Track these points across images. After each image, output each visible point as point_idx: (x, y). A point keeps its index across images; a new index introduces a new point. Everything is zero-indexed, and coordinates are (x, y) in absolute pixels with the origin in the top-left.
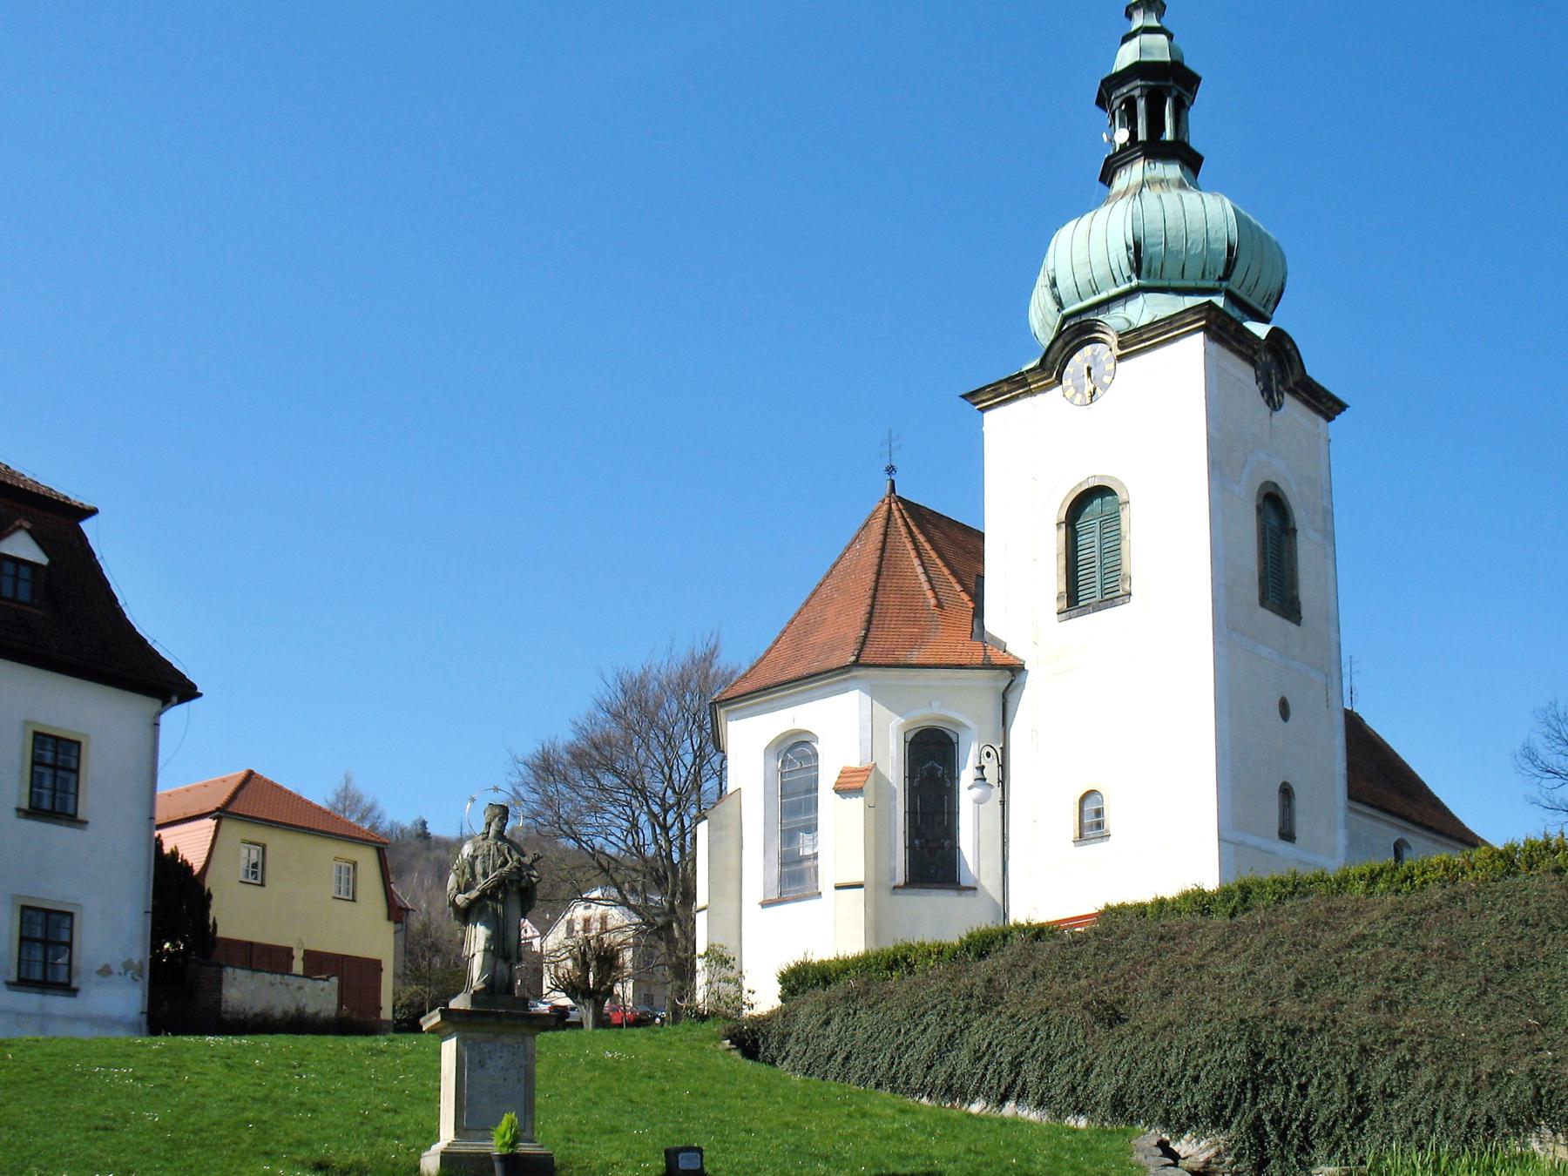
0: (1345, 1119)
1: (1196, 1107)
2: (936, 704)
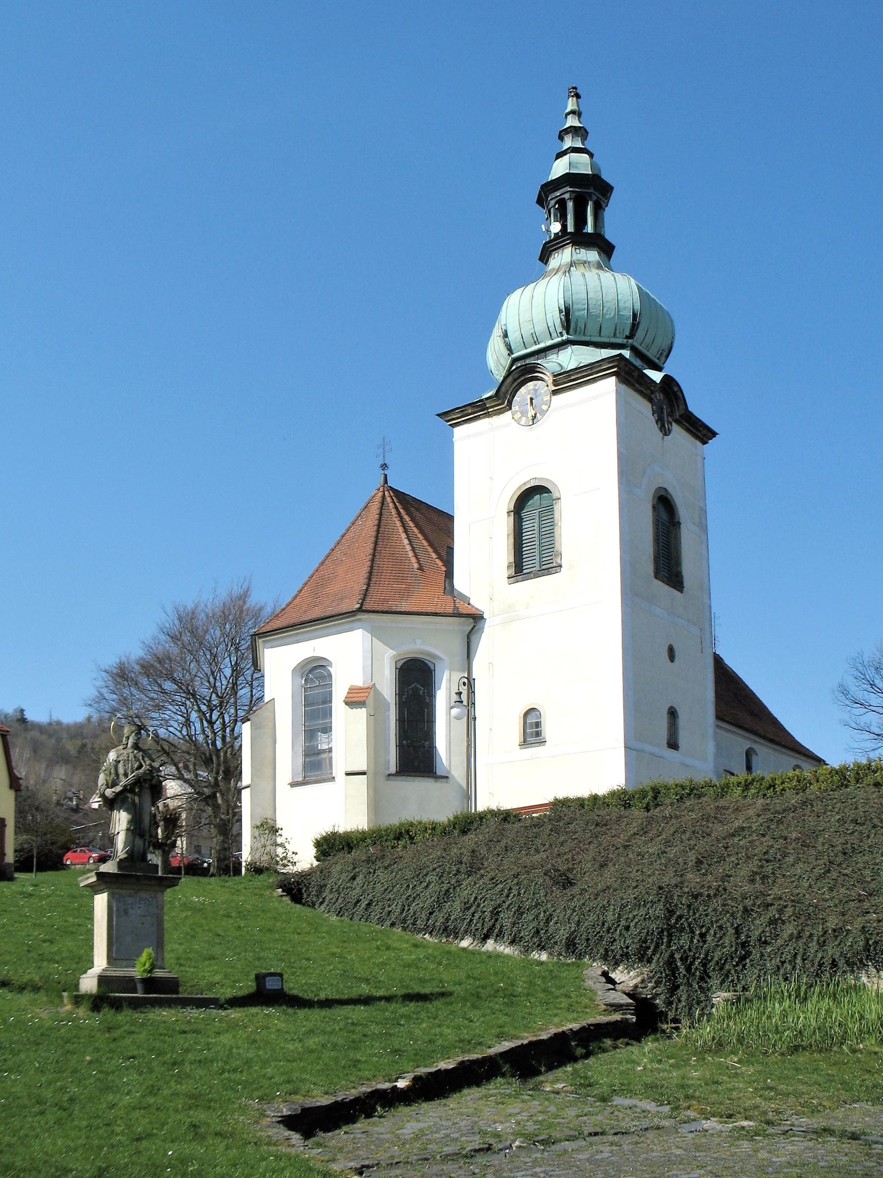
0: (732, 958)
1: (627, 947)
2: (419, 641)
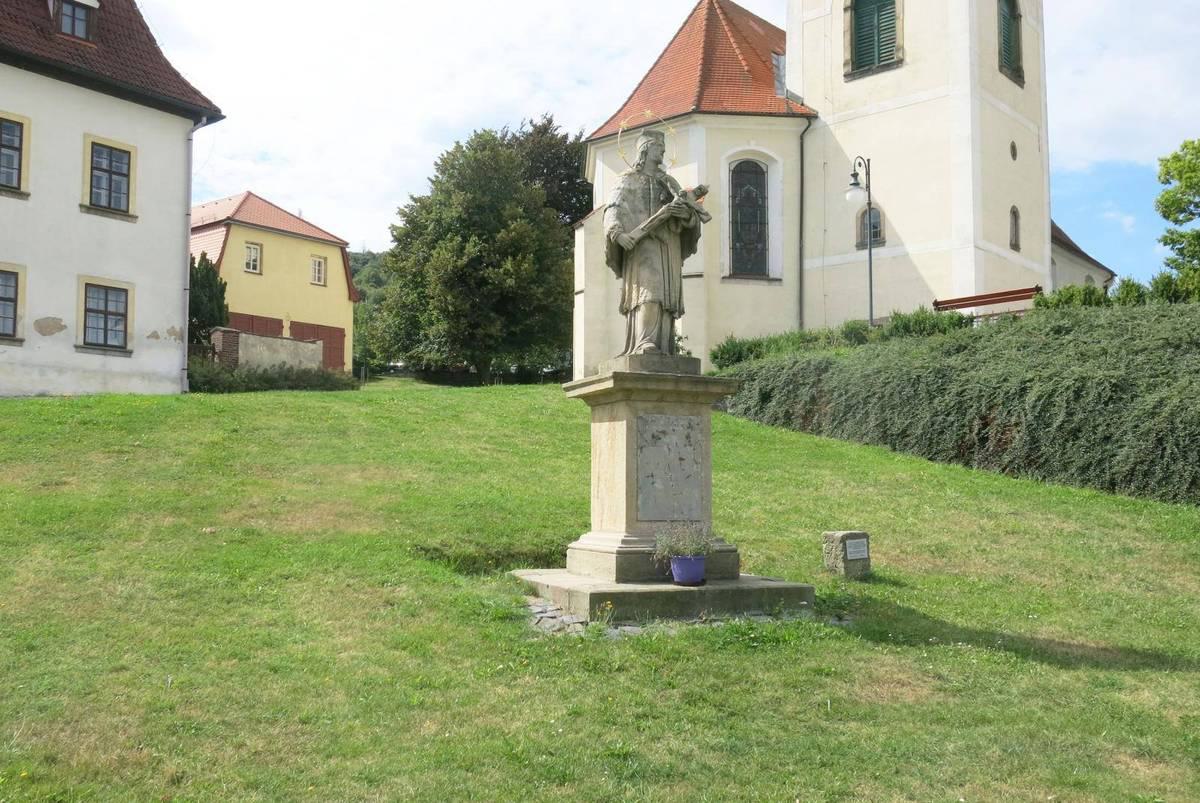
2: (753, 142)
